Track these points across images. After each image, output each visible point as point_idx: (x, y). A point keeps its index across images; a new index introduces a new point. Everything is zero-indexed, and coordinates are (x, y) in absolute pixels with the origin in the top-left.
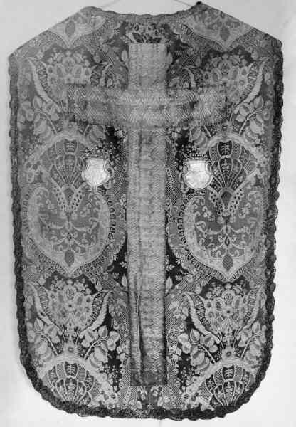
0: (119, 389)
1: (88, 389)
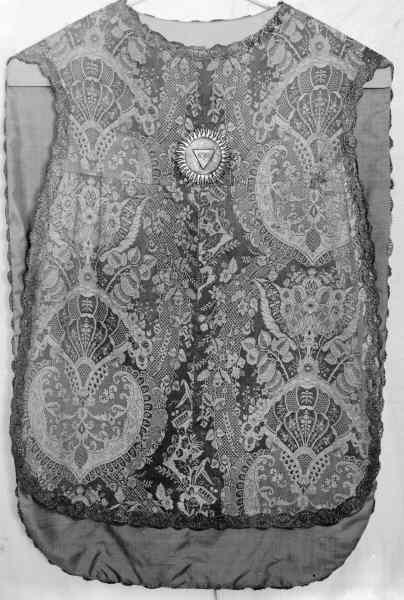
1: (110, 333)
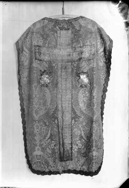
0: (52, 77)
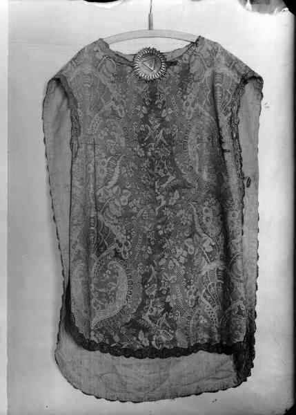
0: (131, 238)
